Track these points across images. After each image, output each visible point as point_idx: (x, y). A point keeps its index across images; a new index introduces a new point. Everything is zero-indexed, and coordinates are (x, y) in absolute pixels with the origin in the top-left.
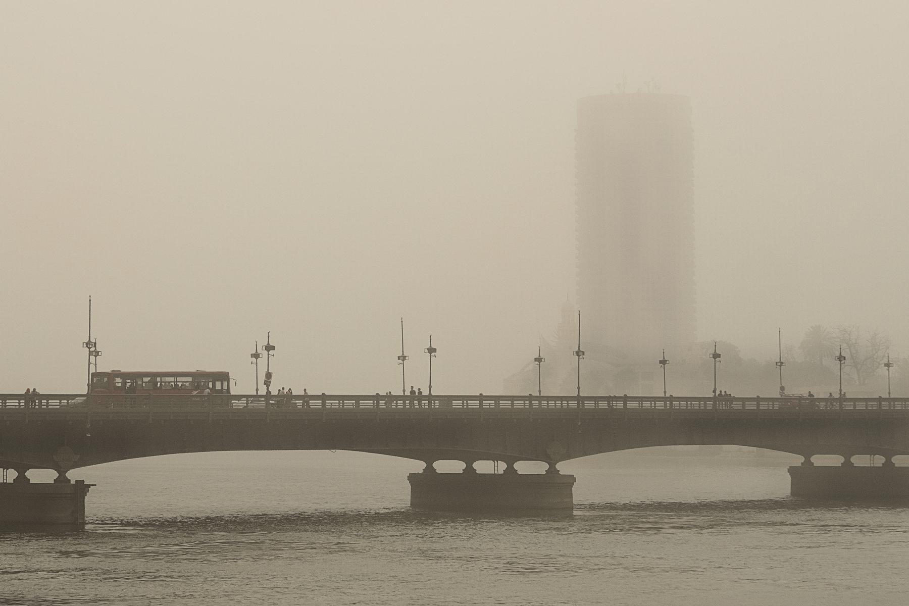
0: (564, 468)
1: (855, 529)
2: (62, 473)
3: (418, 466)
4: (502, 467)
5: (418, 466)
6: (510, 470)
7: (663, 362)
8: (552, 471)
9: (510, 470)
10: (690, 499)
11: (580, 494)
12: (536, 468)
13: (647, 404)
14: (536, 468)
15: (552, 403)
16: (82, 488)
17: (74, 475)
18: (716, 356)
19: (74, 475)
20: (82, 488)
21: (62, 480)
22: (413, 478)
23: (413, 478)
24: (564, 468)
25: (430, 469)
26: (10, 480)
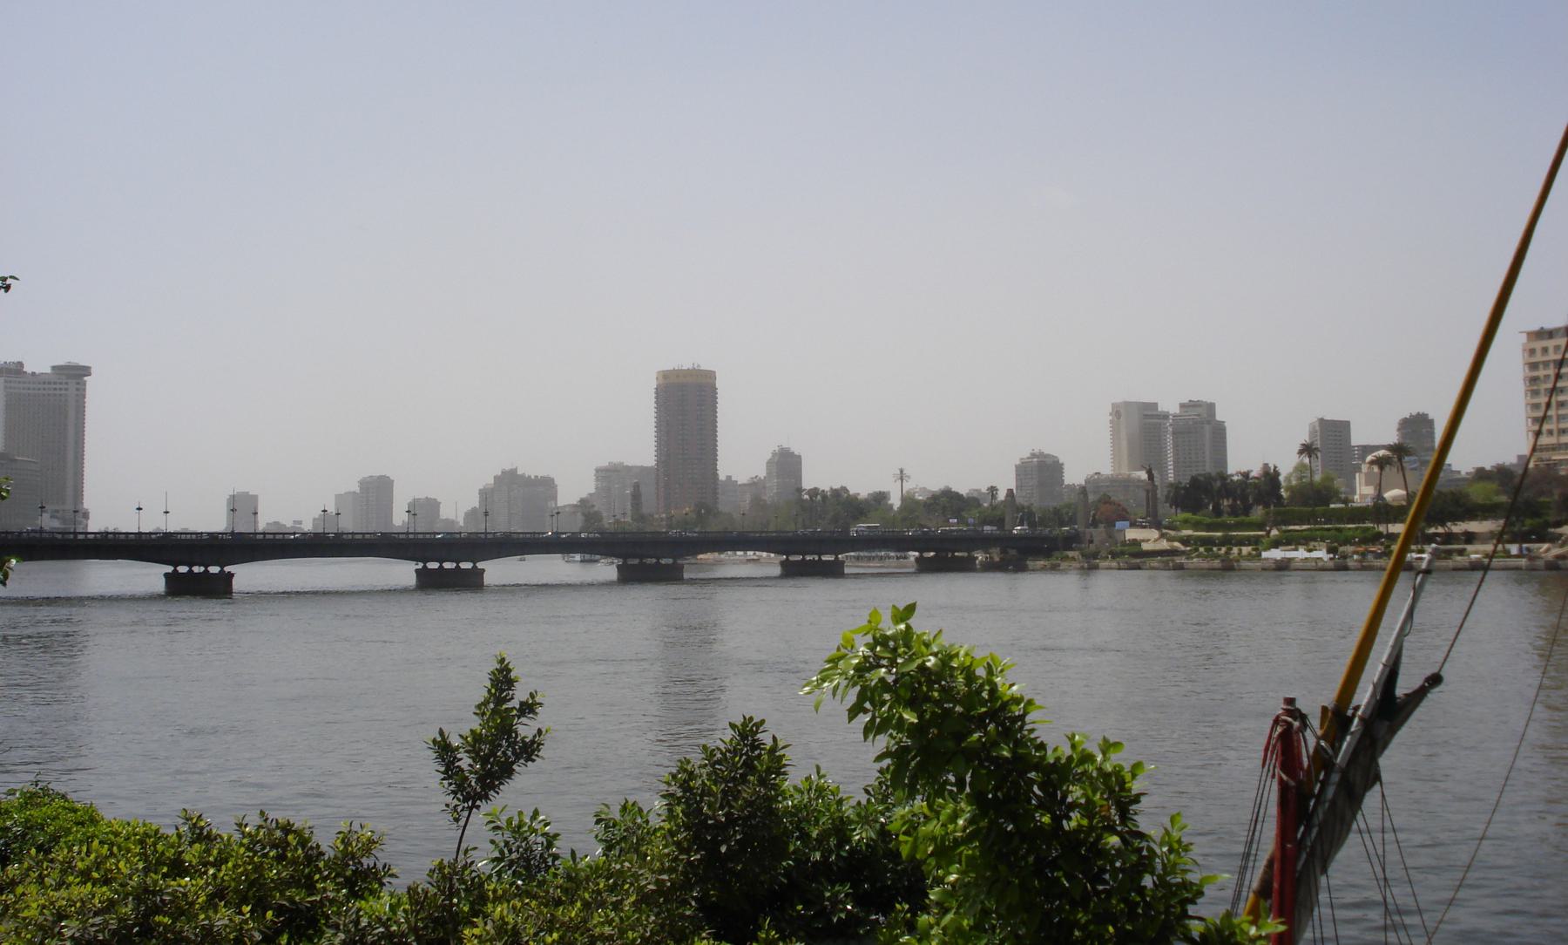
0: (480, 565)
1: (1155, 562)
2: (222, 568)
3: (170, 569)
4: (202, 569)
5: (170, 569)
6: (458, 567)
7: (139, 509)
8: (475, 567)
9: (458, 567)
10: (534, 581)
11: (488, 579)
12: (830, 558)
13: (428, 536)
14: (830, 558)
15: (521, 536)
16: (231, 575)
17: (227, 569)
18: (325, 511)
19: (227, 569)
20: (231, 575)
21: (222, 571)
22: (166, 575)
23: (166, 575)
24: (480, 565)
25: (175, 571)
26: (454, 567)
